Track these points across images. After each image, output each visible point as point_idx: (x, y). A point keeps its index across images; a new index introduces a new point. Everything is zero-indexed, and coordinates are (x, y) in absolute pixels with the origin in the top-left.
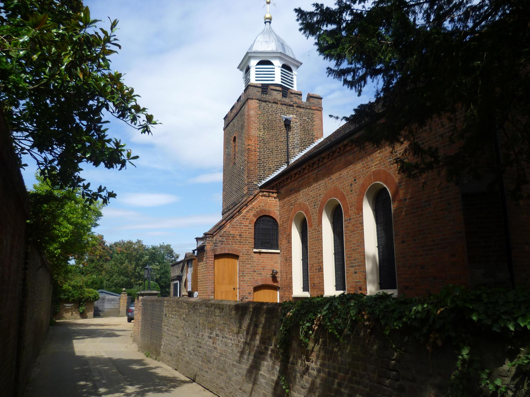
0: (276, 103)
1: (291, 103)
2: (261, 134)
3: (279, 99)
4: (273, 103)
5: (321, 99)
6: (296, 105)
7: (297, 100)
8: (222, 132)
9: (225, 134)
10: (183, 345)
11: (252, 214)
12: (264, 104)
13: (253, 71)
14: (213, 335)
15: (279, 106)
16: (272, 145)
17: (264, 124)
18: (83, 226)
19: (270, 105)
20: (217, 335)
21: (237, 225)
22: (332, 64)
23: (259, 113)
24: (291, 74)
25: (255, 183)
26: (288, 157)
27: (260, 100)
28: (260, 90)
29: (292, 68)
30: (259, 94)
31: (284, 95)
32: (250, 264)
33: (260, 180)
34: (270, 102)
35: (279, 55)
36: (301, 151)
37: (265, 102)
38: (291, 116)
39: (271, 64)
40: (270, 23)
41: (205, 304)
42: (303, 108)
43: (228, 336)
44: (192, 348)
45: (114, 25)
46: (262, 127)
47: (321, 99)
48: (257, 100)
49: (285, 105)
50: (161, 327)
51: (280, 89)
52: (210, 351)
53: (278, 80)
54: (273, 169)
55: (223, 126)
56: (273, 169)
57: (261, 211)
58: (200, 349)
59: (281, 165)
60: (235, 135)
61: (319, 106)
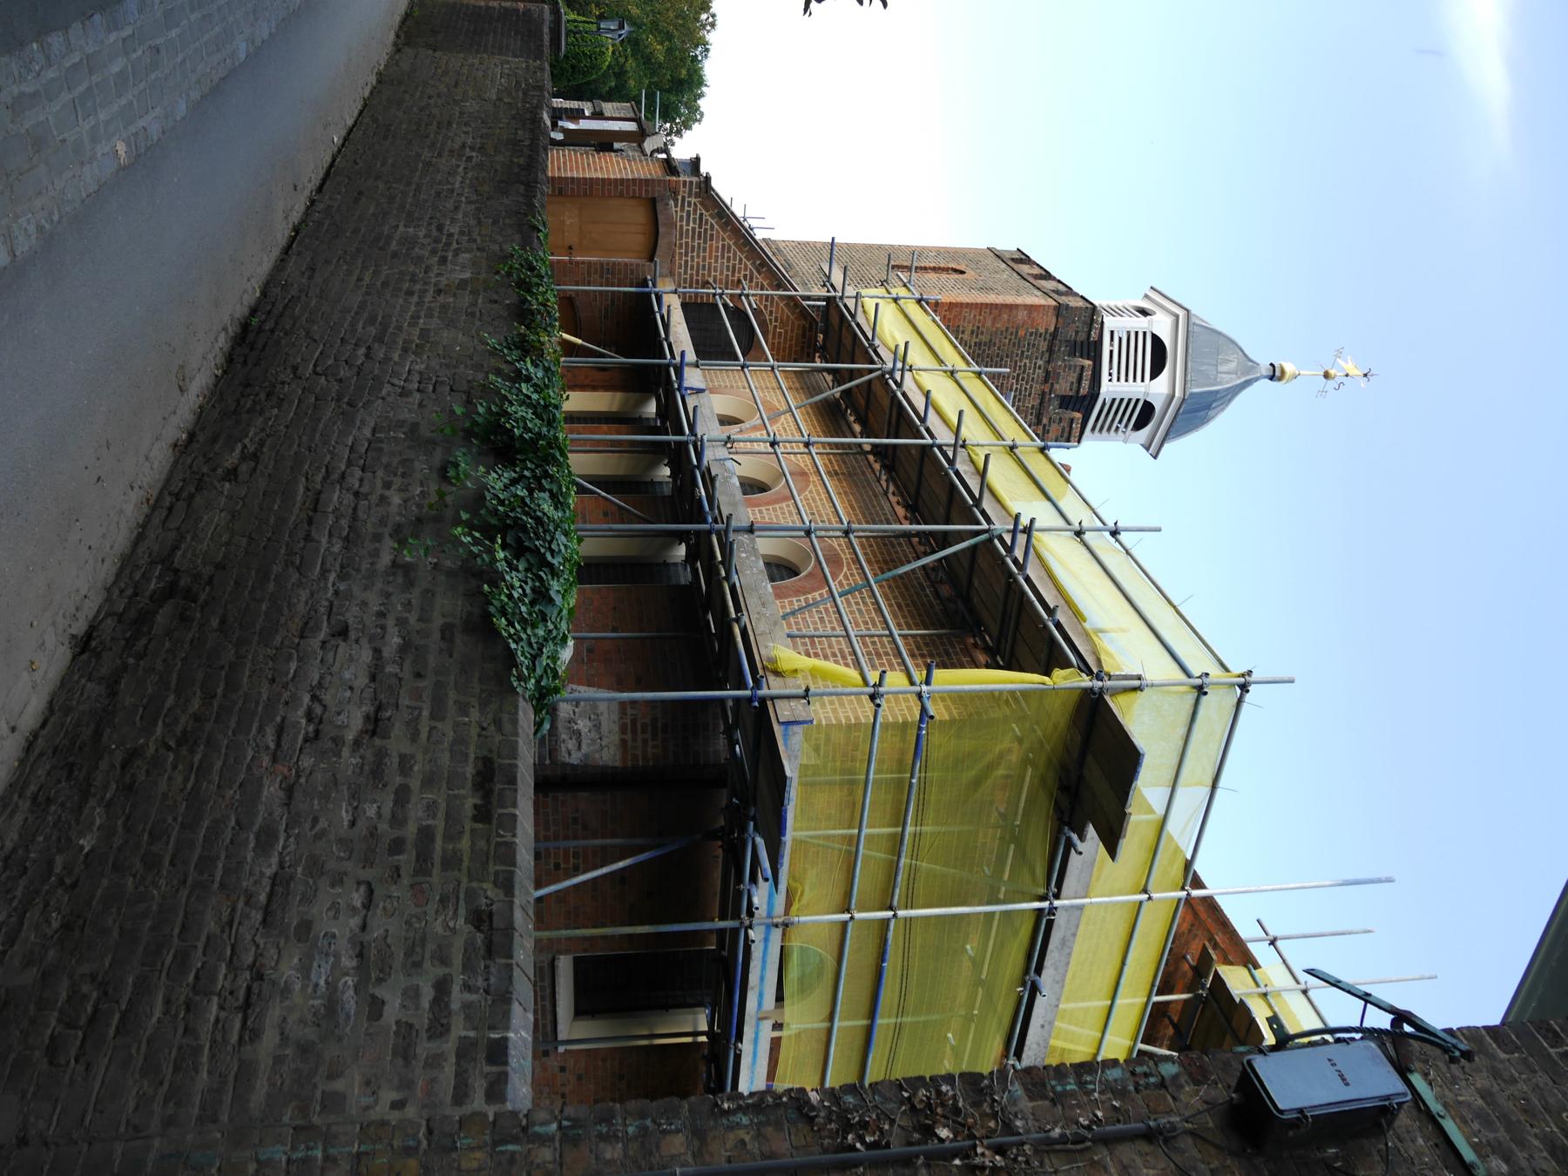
0: (1046, 380)
1: (1045, 421)
3: (1057, 386)
4: (1047, 373)
8: (982, 244)
9: (976, 251)
10: (439, 95)
12: (1044, 346)
13: (1141, 323)
14: (468, 152)
15: (1037, 388)
17: (990, 344)
19: (1040, 362)
20: (470, 159)
23: (1021, 333)
27: (1054, 335)
28: (1082, 336)
29: (1145, 432)
30: (1071, 334)
31: (1066, 402)
32: (634, 740)
35: (1177, 394)
37: (1050, 350)
39: (1154, 375)
40: (1272, 378)
41: (288, 805)
43: (470, 175)
44: (435, 111)
46: (984, 338)
48: (1056, 329)
49: (1041, 403)
50: (477, 52)
51: (1083, 392)
52: (433, 145)
53: (1110, 388)
55: (1001, 246)
58: (434, 126)
60: (968, 271)
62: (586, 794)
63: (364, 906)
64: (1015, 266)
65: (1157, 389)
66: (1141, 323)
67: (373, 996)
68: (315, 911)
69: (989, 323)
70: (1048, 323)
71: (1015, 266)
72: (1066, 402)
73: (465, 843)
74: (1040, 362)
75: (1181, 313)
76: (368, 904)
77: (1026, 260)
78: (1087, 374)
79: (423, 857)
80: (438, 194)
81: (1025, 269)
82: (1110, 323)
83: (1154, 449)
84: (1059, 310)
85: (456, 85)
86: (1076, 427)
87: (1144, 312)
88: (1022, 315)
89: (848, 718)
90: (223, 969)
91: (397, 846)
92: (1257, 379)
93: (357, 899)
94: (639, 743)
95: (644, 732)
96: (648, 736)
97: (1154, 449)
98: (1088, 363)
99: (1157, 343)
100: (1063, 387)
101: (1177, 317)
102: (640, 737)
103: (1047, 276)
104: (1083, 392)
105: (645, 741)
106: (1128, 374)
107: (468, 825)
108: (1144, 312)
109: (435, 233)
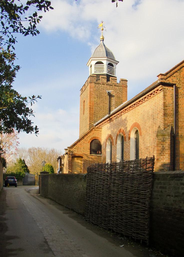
0: (104, 84)
1: (112, 84)
2: (96, 100)
4: (103, 84)
5: (127, 81)
6: (114, 85)
7: (115, 83)
11: (89, 139)
12: (97, 85)
13: (93, 67)
15: (105, 86)
16: (101, 105)
17: (97, 95)
18: (83, 215)
19: (101, 86)
21: (82, 144)
22: (29, 117)
24: (113, 68)
25: (92, 124)
26: (110, 111)
27: (95, 83)
29: (114, 64)
31: (108, 80)
32: (165, 159)
33: (95, 122)
34: (100, 84)
36: (116, 108)
38: (111, 91)
42: (118, 86)
45: (16, 38)
46: (96, 97)
47: (127, 81)
50: (48, 185)
54: (101, 117)
56: (101, 117)
57: (94, 137)
59: (106, 115)
61: (126, 85)
62: (176, 168)
63: (169, 196)
64: (83, 91)
65: (105, 62)
66: (93, 67)
67: (182, 194)
68: (170, 203)
69: (93, 96)
70: (93, 85)
71: (83, 91)
72: (108, 80)
73: (162, 182)
74: (101, 86)
75: (91, 59)
76: (169, 196)
77: (82, 89)
78: (103, 76)
79: (163, 188)
80: (70, 191)
81: (84, 89)
82: (93, 73)
83: (117, 63)
84: (91, 83)
85: (53, 188)
86: (113, 78)
87: (91, 66)
88: (92, 90)
89: (163, 120)
90: (177, 216)
91: (161, 192)
92: (103, 43)
93: (168, 197)
94: (166, 158)
95: (164, 157)
96: (165, 157)
97: (117, 63)
98: (101, 77)
99: (98, 63)
100: (105, 81)
101: (92, 60)
102: (165, 158)
103: (85, 85)
104: (106, 77)
105: (166, 157)
106: (103, 69)
107: (160, 181)
108: (91, 66)
109: (75, 191)
